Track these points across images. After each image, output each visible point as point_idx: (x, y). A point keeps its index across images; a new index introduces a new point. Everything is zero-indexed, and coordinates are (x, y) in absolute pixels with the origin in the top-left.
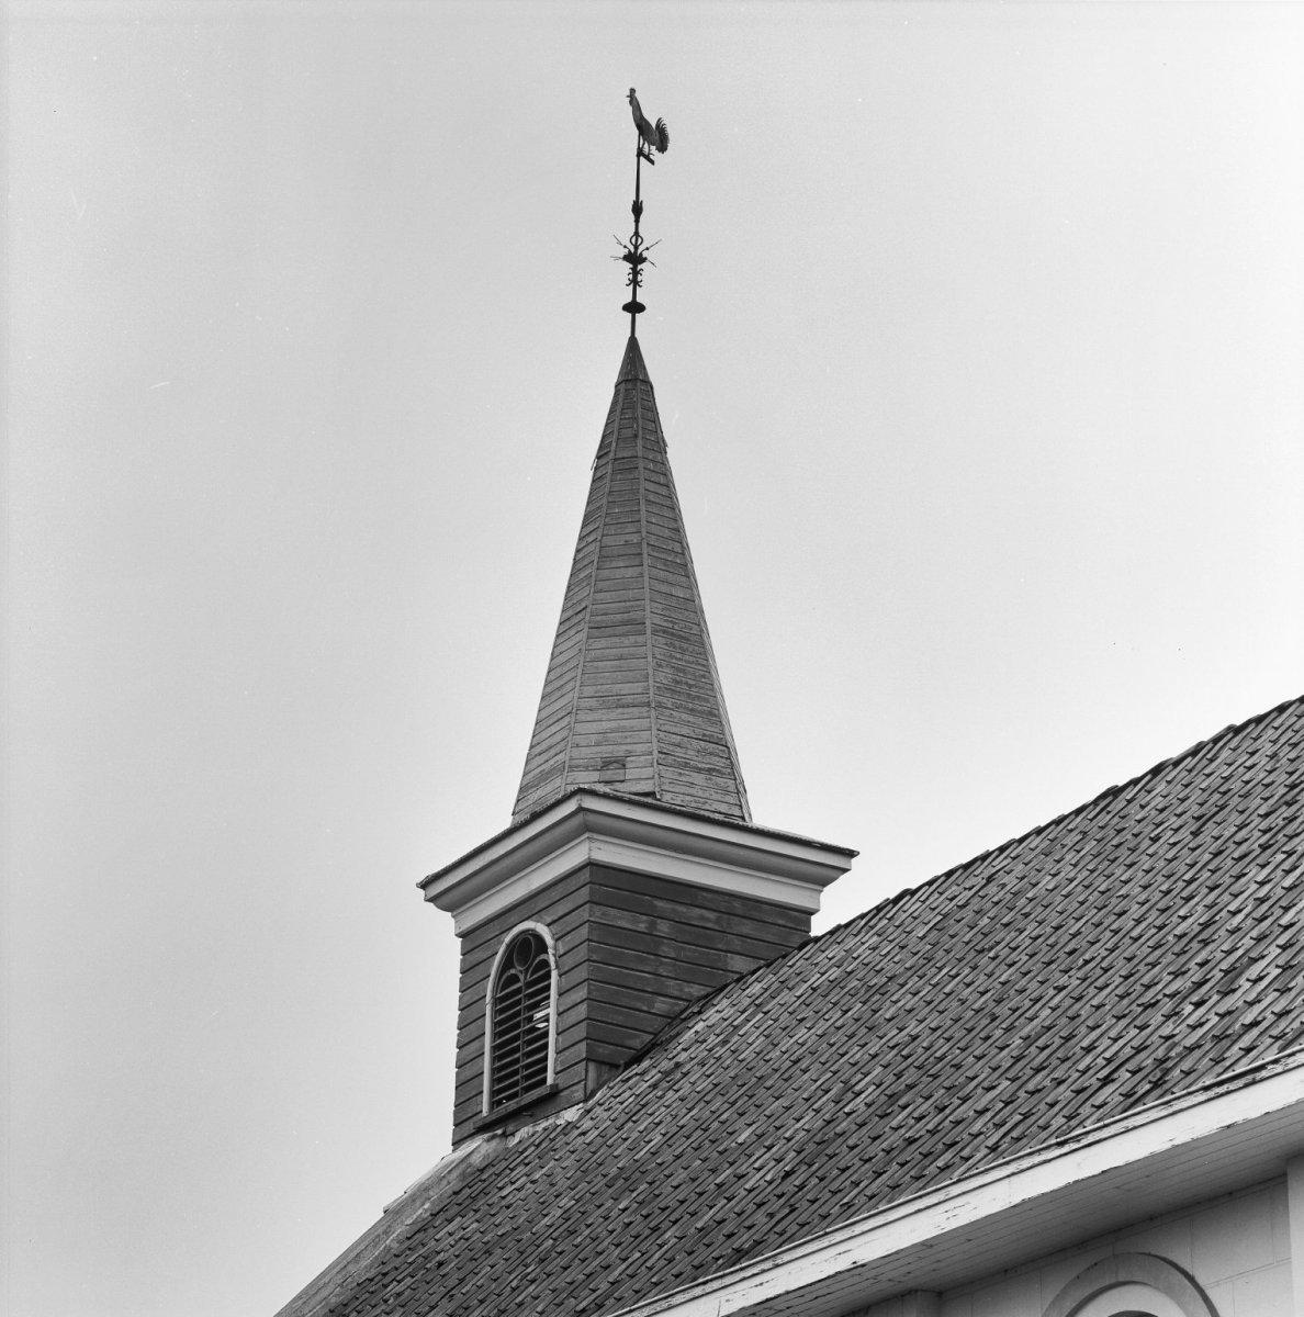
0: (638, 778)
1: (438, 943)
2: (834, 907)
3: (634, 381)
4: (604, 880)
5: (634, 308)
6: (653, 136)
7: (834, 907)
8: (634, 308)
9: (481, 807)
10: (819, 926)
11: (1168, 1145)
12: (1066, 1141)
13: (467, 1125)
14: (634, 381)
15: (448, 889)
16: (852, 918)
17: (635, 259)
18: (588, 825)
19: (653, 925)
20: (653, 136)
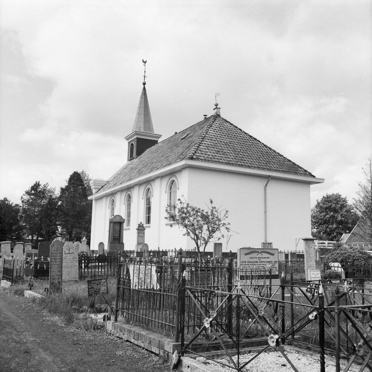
10: (158, 142)
13: (131, 157)
17: (144, 77)
20: (145, 62)
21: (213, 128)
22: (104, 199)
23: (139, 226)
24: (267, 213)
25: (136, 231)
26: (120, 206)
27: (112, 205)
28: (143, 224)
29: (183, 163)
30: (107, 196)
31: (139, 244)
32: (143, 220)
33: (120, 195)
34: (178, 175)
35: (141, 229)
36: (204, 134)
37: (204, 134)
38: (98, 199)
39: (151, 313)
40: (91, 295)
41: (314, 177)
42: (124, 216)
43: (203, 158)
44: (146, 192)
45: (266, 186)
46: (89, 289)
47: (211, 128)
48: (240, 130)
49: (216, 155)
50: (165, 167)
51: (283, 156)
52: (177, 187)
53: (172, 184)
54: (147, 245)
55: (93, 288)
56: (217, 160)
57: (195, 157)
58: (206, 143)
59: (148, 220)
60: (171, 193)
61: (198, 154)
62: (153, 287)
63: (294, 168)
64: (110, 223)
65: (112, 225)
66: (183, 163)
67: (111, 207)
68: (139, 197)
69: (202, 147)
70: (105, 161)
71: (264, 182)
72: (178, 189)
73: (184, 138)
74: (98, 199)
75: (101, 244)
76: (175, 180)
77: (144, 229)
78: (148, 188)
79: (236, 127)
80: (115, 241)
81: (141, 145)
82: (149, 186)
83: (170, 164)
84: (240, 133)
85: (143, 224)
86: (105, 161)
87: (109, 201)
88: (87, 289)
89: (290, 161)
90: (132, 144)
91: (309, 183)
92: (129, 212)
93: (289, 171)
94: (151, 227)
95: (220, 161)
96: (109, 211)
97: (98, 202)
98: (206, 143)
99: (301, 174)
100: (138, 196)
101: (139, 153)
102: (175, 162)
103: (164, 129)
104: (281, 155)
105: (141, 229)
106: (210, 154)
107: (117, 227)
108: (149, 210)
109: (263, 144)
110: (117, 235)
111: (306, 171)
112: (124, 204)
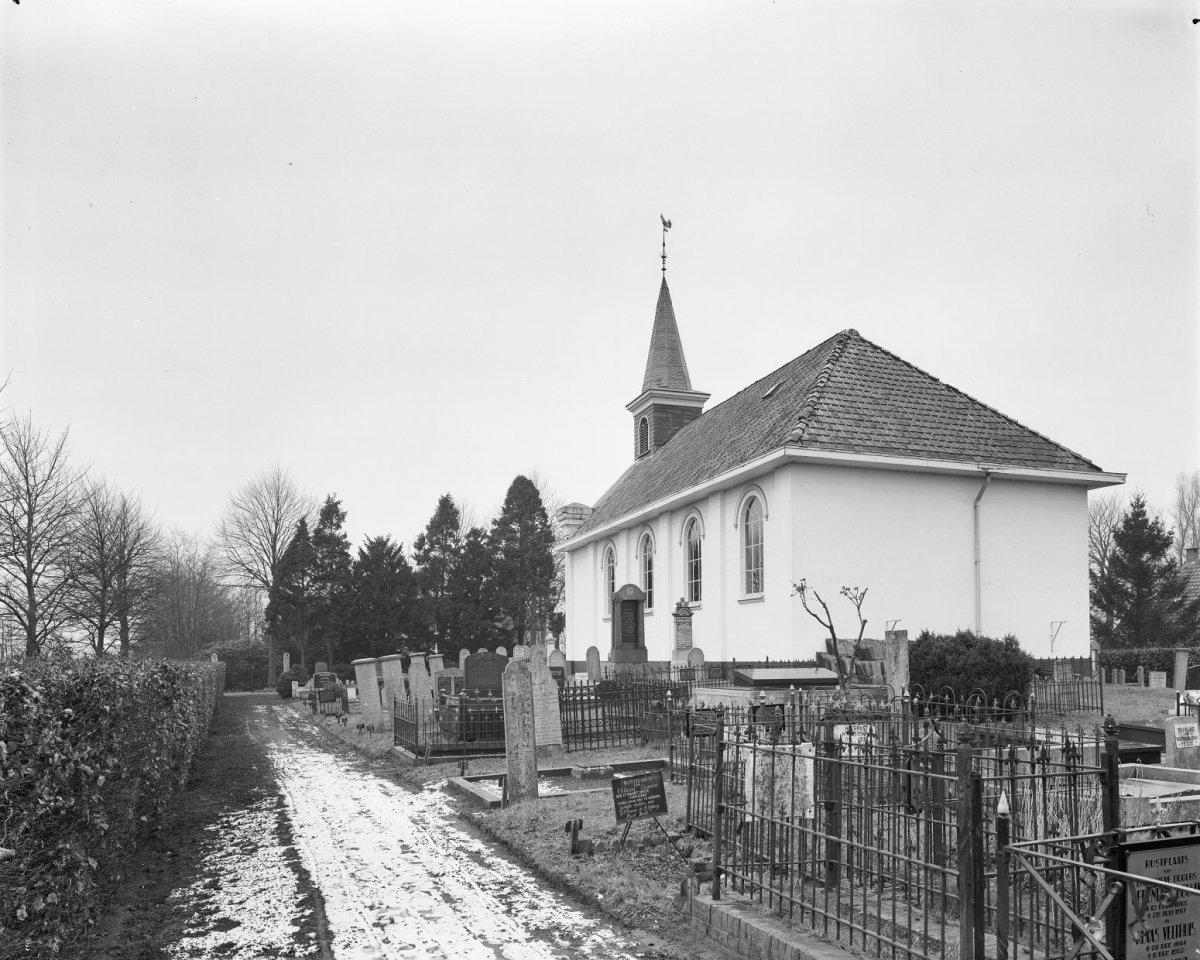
0: (664, 383)
1: (630, 416)
2: (707, 406)
3: (664, 288)
4: (658, 408)
5: (664, 269)
6: (667, 224)
7: (707, 406)
8: (664, 269)
9: (636, 390)
10: (703, 411)
11: (609, 625)
12: (678, 491)
13: (643, 451)
14: (664, 288)
15: (631, 407)
16: (981, 543)
17: (664, 257)
18: (653, 396)
19: (1182, 704)
20: (667, 224)
21: (843, 364)
22: (590, 551)
23: (679, 607)
24: (982, 564)
25: (673, 618)
26: (628, 562)
27: (646, 547)
28: (687, 604)
29: (778, 453)
30: (595, 542)
31: (679, 649)
32: (682, 591)
33: (625, 540)
34: (766, 486)
35: (683, 614)
36: (822, 382)
37: (823, 379)
38: (574, 551)
39: (701, 795)
40: (625, 816)
41: (1099, 470)
42: (640, 584)
43: (825, 439)
44: (744, 507)
45: (979, 498)
46: (617, 801)
47: (838, 364)
48: (908, 365)
49: (857, 429)
50: (729, 467)
51: (1016, 423)
52: (764, 514)
53: (750, 506)
54: (699, 652)
55: (626, 798)
56: (860, 442)
57: (806, 436)
58: (829, 401)
59: (696, 592)
60: (747, 526)
61: (813, 431)
62: (124, 505)
63: (1045, 451)
64: (614, 604)
65: (618, 608)
66: (778, 453)
67: (606, 565)
68: (628, 557)
69: (821, 413)
70: (585, 457)
71: (970, 491)
72: (767, 517)
73: (769, 395)
74: (574, 551)
75: (593, 652)
76: (757, 495)
77: (691, 615)
78: (751, 497)
79: (897, 359)
80: (627, 644)
81: (666, 416)
82: (694, 515)
83: (743, 460)
84: (908, 374)
85: (687, 604)
86: (585, 457)
87: (635, 544)
88: (613, 804)
89: (1035, 434)
90: (644, 420)
91: (1084, 487)
92: (650, 575)
93: (1033, 457)
94: (703, 606)
95: (868, 443)
96: (602, 577)
97: (578, 556)
98: (829, 401)
99: (1065, 466)
100: (669, 543)
101: (660, 442)
102: (755, 454)
103: (718, 375)
104: (1011, 422)
105: (683, 614)
106: (841, 428)
107: (629, 610)
108: (695, 571)
109: (966, 395)
110: (631, 631)
111: (1077, 457)
112: (681, 543)
